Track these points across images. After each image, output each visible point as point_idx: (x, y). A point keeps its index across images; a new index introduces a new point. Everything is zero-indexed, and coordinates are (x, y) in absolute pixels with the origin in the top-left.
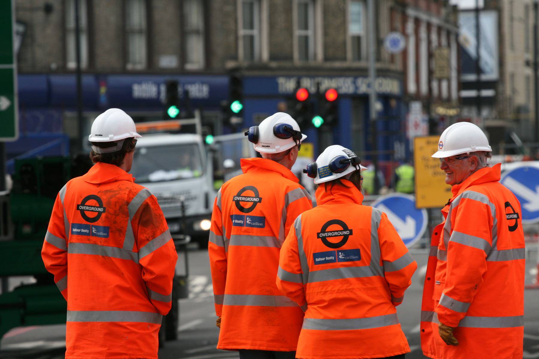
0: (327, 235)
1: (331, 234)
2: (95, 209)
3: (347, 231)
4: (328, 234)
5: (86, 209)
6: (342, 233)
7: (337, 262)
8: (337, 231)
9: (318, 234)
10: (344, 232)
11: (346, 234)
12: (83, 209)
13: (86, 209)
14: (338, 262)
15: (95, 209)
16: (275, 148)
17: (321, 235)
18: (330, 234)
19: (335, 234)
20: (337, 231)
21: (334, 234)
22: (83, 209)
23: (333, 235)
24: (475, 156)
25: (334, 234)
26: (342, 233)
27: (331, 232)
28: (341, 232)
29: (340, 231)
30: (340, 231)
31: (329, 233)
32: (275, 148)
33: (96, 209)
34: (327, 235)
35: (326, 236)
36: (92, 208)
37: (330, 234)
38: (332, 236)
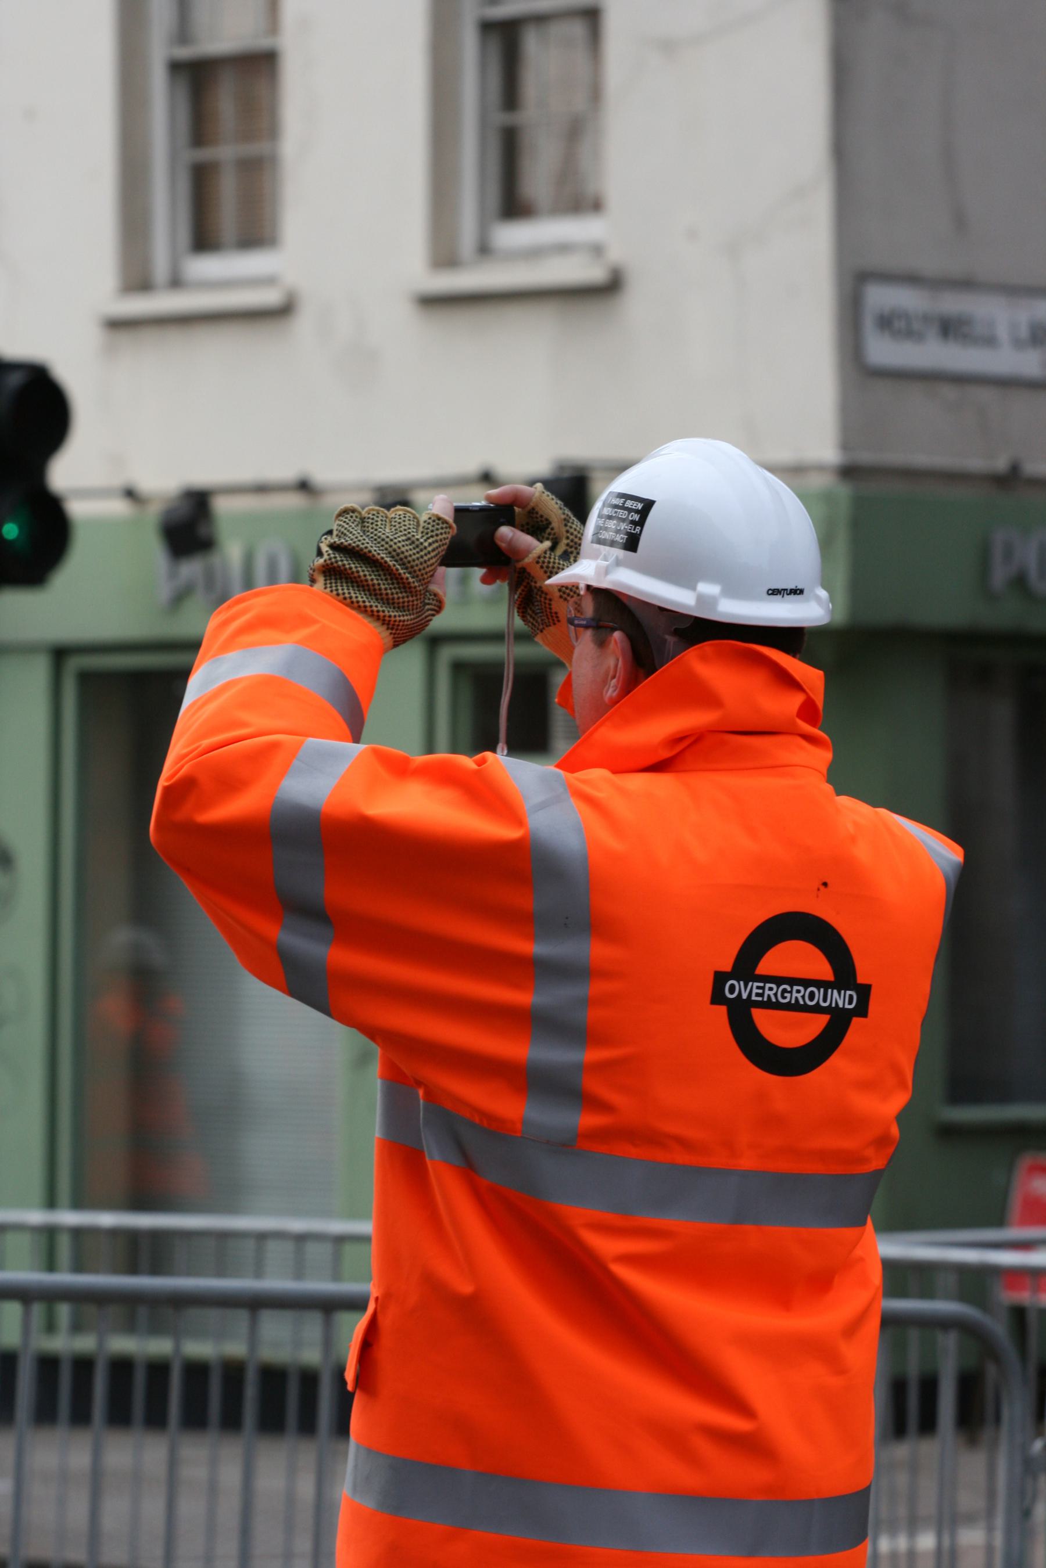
0: (757, 995)
1: (803, 997)
2: (812, 996)
3: (848, 992)
4: (763, 988)
5: (762, 995)
6: (825, 1000)
7: (357, 1500)
8: (806, 983)
9: (720, 978)
10: (835, 992)
11: (841, 1005)
12: (745, 996)
13: (762, 995)
14: (890, 1322)
15: (812, 996)
16: (693, 588)
17: (732, 989)
18: (771, 991)
19: (795, 994)
20: (806, 983)
21: (788, 995)
22: (745, 996)
23: (784, 1001)
24: (608, 563)
25: (788, 995)
26: (825, 1000)
27: (778, 981)
28: (822, 990)
29: (819, 984)
30: (819, 984)
31: (768, 985)
32: (693, 588)
33: (819, 994)
34: (757, 995)
35: (754, 998)
36: (795, 988)
37: (771, 991)
38: (777, 1006)
